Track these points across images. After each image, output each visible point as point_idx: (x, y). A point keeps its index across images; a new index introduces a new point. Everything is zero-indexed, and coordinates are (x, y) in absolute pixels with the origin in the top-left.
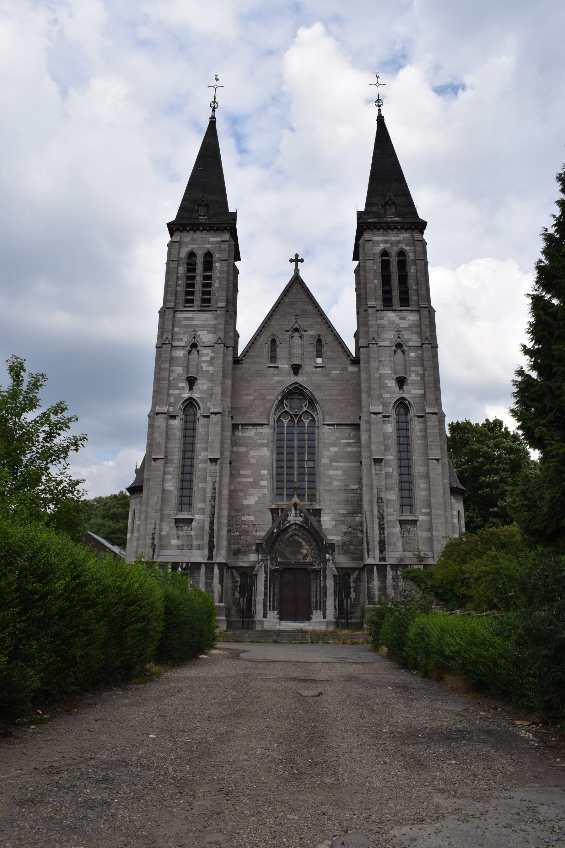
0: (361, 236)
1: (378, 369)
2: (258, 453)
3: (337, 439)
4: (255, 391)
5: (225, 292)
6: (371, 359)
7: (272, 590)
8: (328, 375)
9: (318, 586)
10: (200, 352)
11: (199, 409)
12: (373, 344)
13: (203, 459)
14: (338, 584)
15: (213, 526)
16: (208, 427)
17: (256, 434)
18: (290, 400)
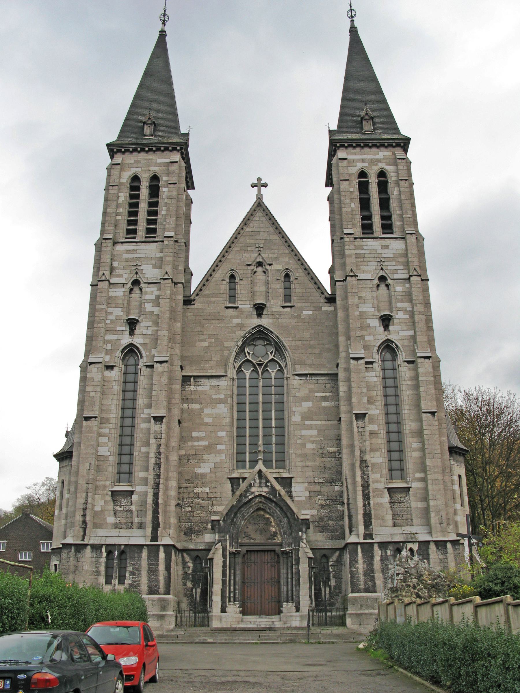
0: (334, 156)
1: (357, 306)
2: (214, 411)
3: (310, 392)
4: (210, 336)
5: (174, 219)
6: (349, 294)
7: (232, 577)
8: (298, 316)
9: (289, 571)
10: (143, 290)
11: (142, 357)
12: (352, 276)
13: (146, 418)
14: (313, 568)
15: (158, 499)
16: (152, 379)
17: (212, 387)
18: (252, 347)
